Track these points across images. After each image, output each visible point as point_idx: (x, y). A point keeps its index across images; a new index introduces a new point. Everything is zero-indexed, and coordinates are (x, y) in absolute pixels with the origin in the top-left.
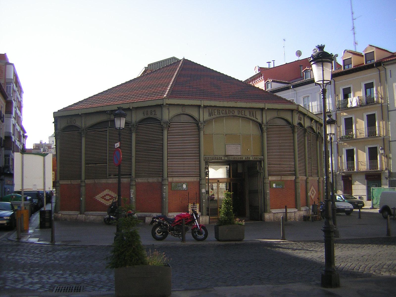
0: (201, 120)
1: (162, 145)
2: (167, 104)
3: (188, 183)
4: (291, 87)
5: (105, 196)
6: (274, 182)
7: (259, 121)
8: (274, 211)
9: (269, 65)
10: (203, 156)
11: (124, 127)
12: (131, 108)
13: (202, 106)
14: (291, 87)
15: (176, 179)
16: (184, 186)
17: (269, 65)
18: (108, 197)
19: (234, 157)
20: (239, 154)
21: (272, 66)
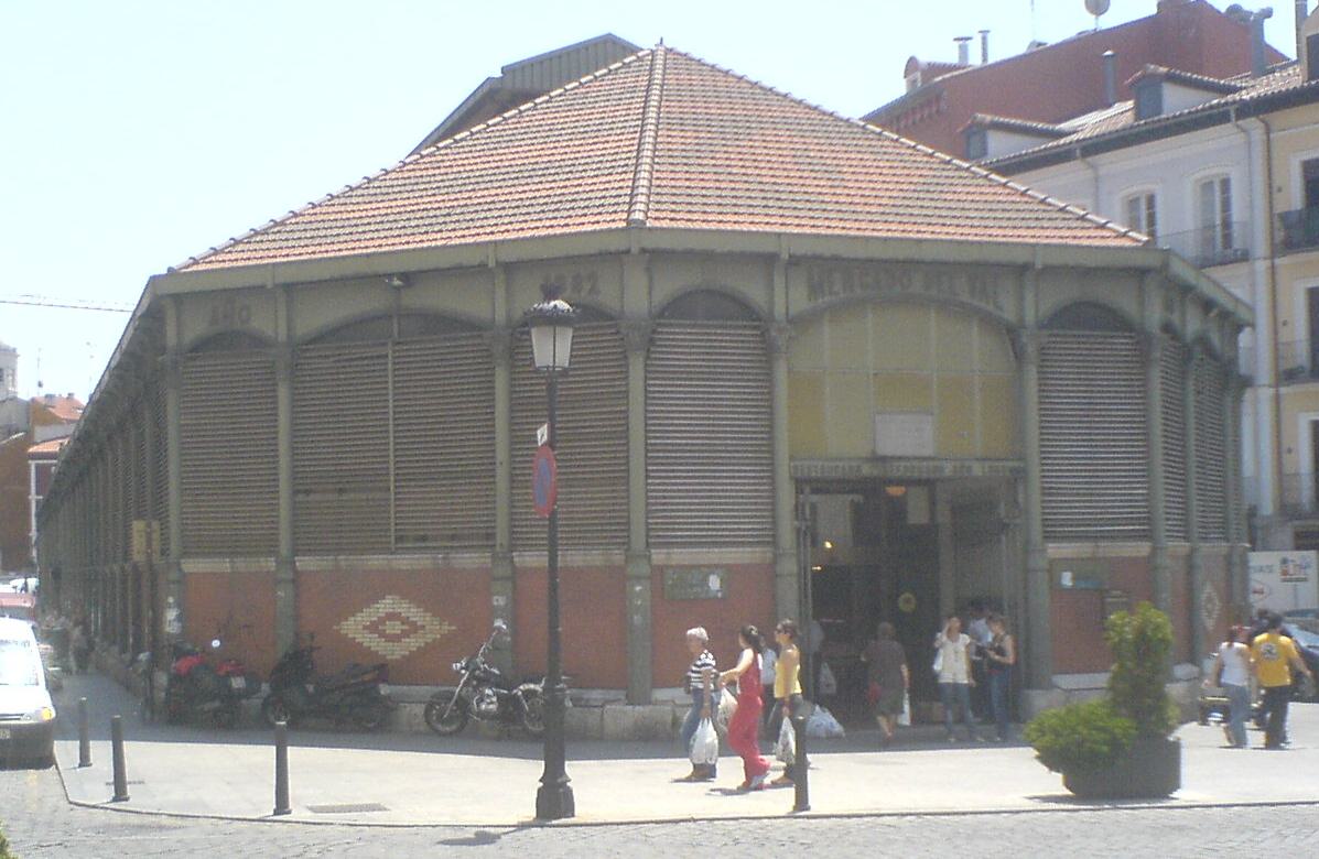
0: (779, 310)
1: (625, 414)
2: (644, 251)
3: (730, 572)
4: (1078, 152)
5: (382, 621)
6: (1068, 563)
7: (1009, 315)
8: (1066, 681)
9: (963, 52)
10: (786, 461)
11: (567, 365)
12: (491, 264)
13: (785, 256)
14: (1078, 152)
15: (680, 556)
16: (714, 583)
17: (963, 52)
18: (394, 628)
19: (908, 464)
20: (928, 452)
21: (975, 60)
